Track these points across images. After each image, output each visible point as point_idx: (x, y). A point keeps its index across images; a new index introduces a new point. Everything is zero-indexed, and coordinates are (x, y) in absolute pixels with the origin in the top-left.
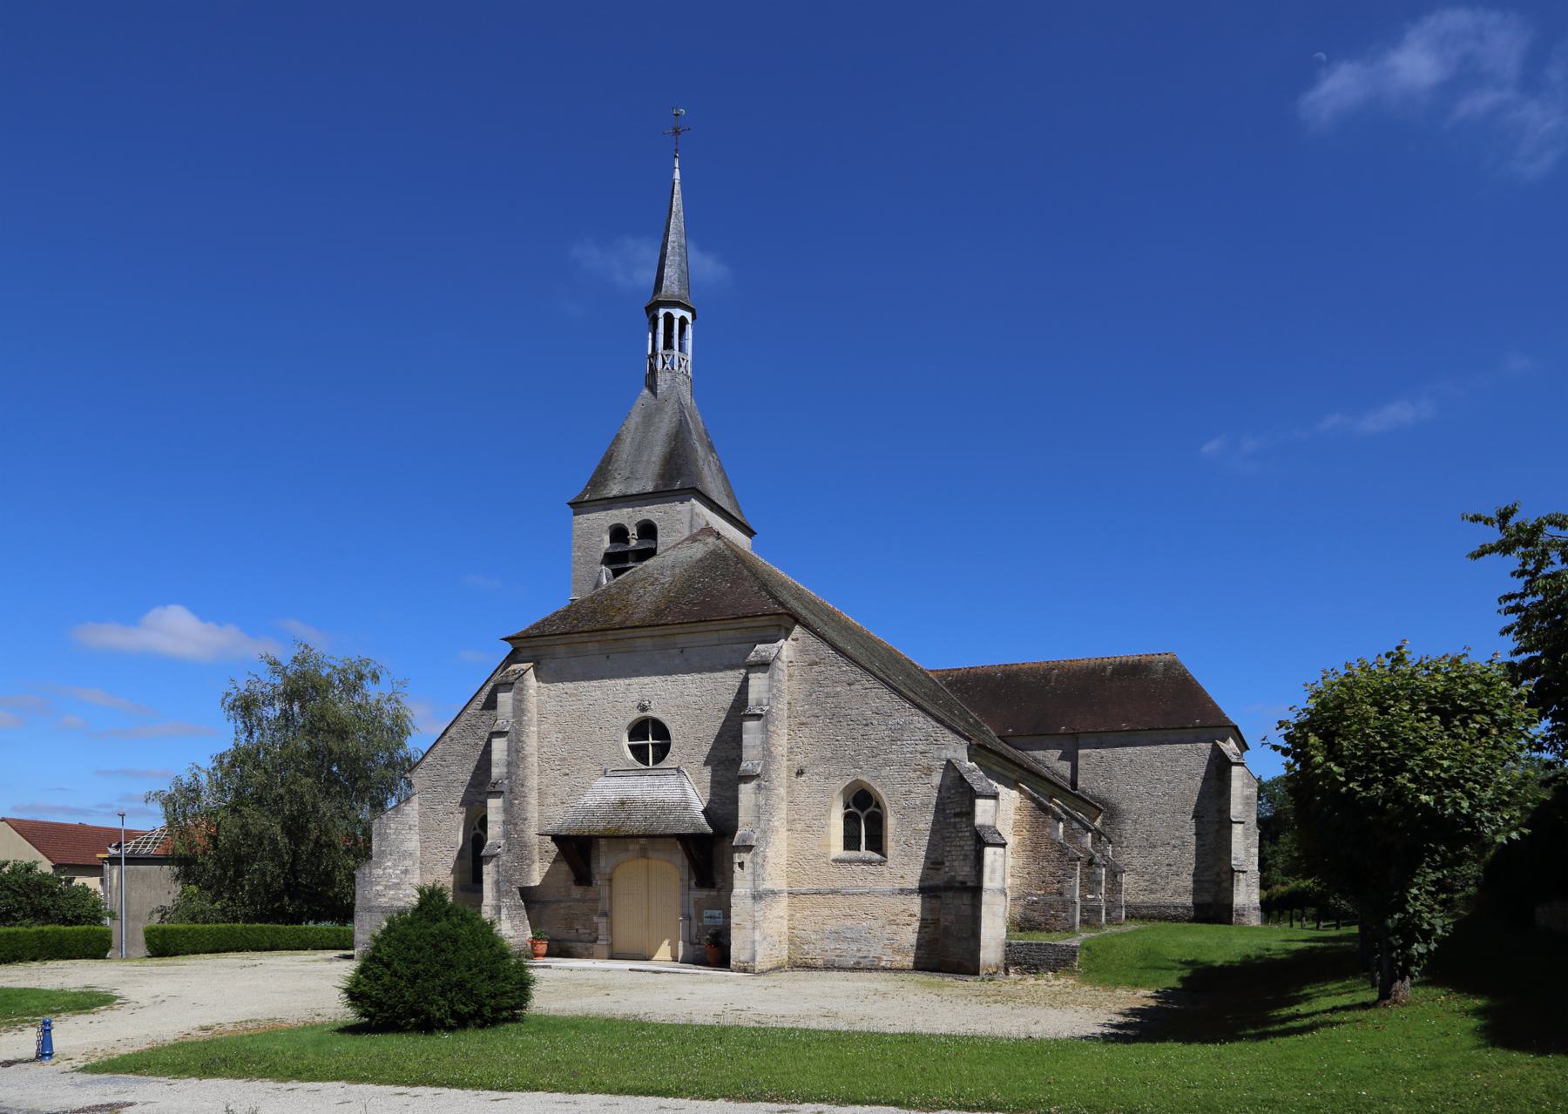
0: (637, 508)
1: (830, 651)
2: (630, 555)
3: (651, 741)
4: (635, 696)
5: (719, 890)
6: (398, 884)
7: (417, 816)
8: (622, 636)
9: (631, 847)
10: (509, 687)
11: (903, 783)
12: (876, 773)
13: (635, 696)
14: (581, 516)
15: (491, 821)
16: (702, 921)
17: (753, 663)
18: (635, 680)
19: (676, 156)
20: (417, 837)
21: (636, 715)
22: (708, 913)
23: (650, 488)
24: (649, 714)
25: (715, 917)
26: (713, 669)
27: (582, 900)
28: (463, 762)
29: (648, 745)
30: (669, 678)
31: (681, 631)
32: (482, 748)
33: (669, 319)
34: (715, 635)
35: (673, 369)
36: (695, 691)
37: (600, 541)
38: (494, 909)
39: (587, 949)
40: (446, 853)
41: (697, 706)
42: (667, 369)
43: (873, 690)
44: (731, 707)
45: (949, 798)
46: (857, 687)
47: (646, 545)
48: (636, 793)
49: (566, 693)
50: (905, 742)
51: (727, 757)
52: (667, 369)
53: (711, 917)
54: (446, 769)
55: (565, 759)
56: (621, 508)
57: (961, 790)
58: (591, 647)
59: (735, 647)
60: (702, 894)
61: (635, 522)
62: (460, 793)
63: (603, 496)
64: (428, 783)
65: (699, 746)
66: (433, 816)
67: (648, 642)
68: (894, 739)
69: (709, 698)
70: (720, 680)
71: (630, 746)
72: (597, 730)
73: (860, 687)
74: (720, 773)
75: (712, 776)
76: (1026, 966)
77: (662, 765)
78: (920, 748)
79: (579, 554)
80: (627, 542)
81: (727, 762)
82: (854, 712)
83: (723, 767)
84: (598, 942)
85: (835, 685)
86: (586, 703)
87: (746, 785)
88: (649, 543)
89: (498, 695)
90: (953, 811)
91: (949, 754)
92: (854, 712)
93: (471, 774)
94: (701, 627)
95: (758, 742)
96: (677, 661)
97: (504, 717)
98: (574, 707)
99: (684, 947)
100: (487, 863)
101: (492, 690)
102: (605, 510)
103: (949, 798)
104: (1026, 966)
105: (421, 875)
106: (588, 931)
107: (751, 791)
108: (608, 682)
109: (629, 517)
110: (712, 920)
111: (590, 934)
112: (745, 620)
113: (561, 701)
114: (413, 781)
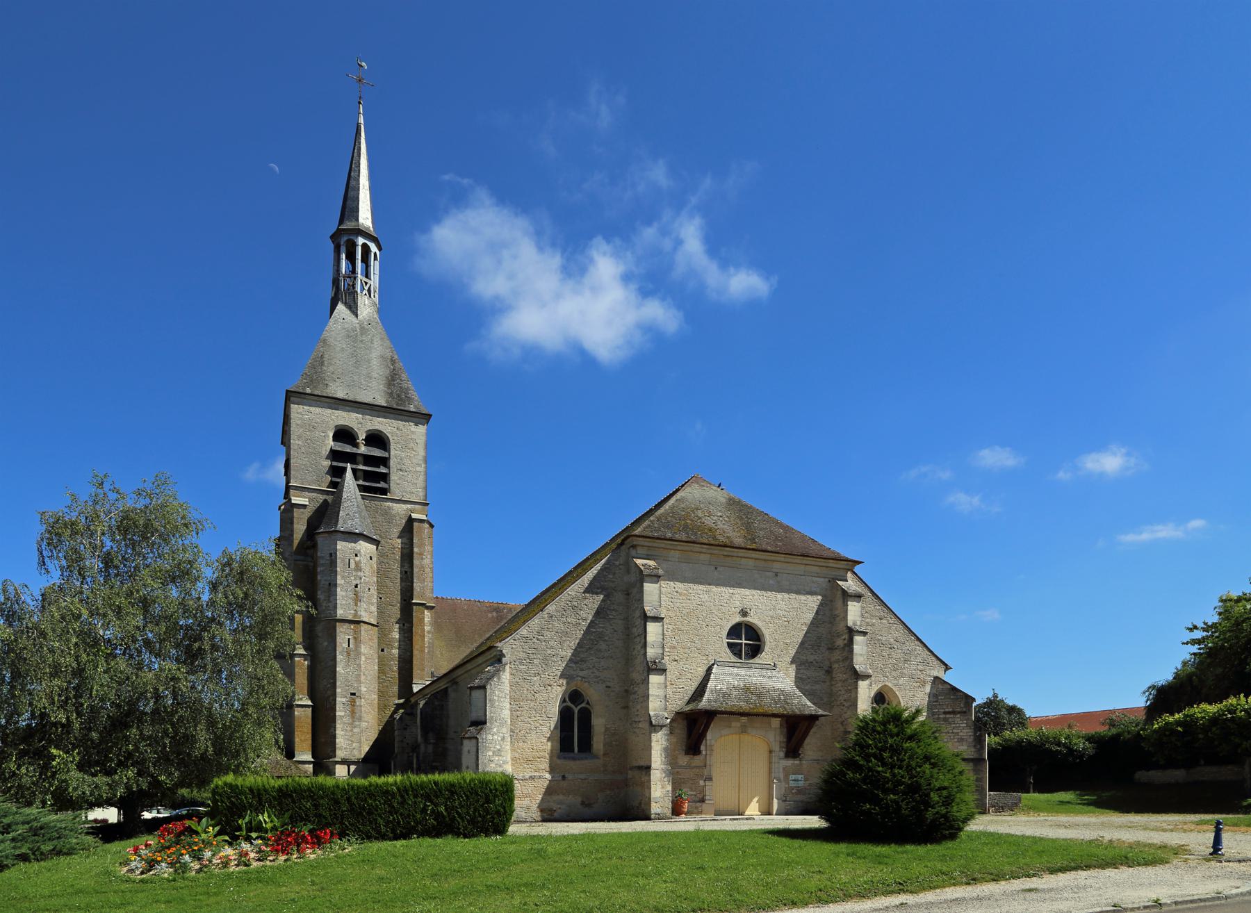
2: (360, 459)
4: (737, 605)
6: (499, 750)
8: (735, 554)
9: (733, 724)
10: (655, 579)
11: (910, 690)
13: (738, 604)
15: (653, 695)
16: (788, 783)
18: (737, 590)
19: (360, 103)
20: (508, 706)
21: (738, 619)
22: (793, 777)
23: (382, 402)
24: (747, 619)
25: (798, 780)
26: (798, 592)
27: (689, 767)
28: (564, 638)
29: (741, 644)
30: (764, 593)
32: (585, 628)
33: (366, 249)
34: (802, 567)
35: (370, 296)
38: (665, 772)
39: (696, 808)
42: (366, 294)
45: (935, 702)
47: (377, 452)
48: (754, 681)
49: (677, 592)
52: (366, 294)
53: (795, 780)
54: (544, 643)
55: (675, 648)
56: (349, 411)
58: (704, 557)
60: (790, 762)
61: (366, 430)
63: (330, 395)
64: (522, 655)
67: (751, 562)
69: (795, 614)
71: (728, 643)
72: (704, 626)
74: (802, 671)
77: (756, 660)
78: (920, 667)
79: (300, 443)
80: (356, 445)
82: (884, 638)
83: (803, 667)
84: (707, 802)
86: (694, 602)
89: (645, 584)
90: (943, 711)
91: (935, 673)
92: (884, 638)
93: (572, 651)
94: (798, 560)
95: (864, 652)
96: (771, 582)
97: (650, 605)
98: (685, 605)
100: (656, 731)
103: (936, 701)
106: (695, 793)
108: (714, 589)
109: (361, 424)
110: (796, 782)
113: (672, 598)
114: (504, 651)
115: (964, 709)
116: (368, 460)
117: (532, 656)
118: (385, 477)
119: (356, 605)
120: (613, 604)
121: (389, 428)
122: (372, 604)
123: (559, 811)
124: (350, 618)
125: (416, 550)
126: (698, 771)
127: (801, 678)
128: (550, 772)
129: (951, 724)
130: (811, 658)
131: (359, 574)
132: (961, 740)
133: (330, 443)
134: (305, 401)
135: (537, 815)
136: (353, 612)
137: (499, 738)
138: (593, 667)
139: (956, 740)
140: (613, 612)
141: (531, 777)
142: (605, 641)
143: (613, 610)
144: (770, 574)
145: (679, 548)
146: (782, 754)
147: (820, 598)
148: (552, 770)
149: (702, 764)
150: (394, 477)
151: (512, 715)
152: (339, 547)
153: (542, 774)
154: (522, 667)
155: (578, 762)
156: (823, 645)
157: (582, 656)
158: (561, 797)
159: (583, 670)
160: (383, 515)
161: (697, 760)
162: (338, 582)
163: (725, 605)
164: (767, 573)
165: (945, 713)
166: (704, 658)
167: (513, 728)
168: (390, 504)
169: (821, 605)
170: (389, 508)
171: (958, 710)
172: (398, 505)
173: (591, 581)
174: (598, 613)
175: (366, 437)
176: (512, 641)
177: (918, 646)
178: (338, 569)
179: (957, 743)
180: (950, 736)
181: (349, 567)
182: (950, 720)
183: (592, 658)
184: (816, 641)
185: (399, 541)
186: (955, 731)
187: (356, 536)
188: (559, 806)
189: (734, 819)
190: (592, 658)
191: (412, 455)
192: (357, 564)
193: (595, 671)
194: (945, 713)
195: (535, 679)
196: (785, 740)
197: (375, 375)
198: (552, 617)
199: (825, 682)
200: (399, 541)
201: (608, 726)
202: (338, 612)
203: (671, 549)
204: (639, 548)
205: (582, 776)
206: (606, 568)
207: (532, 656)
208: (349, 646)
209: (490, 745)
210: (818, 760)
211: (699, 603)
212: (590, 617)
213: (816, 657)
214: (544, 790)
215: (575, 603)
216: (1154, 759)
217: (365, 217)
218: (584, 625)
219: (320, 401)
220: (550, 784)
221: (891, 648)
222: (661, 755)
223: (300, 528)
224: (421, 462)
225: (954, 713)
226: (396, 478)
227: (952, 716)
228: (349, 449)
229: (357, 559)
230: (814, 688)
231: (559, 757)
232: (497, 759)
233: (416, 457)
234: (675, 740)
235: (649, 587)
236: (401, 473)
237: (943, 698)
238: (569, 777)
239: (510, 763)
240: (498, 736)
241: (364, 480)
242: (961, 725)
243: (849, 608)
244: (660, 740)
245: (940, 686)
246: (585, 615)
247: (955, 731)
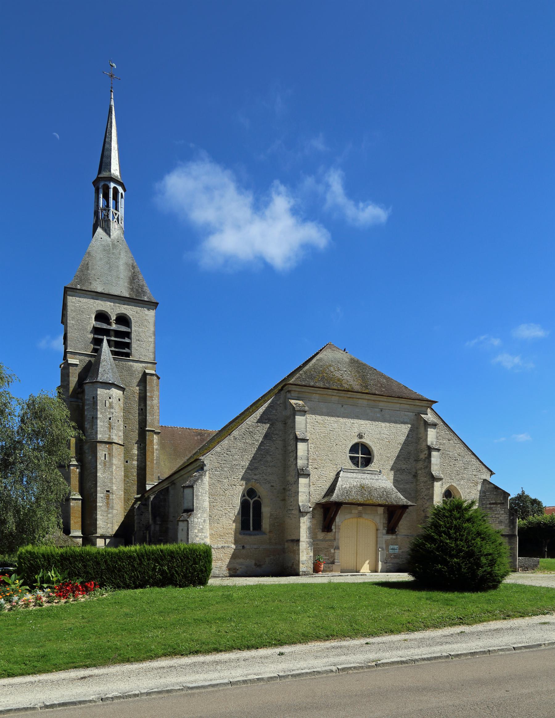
0: (117, 305)
1: (442, 423)
3: (360, 455)
4: (356, 431)
5: (396, 535)
6: (202, 529)
7: (208, 485)
8: (354, 397)
9: (353, 511)
10: (303, 413)
12: (458, 483)
14: (74, 298)
17: (431, 424)
18: (356, 421)
19: (111, 91)
20: (208, 499)
21: (356, 440)
22: (391, 547)
26: (396, 422)
27: (324, 540)
28: (244, 453)
29: (358, 457)
30: (374, 423)
31: (386, 400)
32: (257, 447)
34: (398, 405)
35: (118, 223)
36: (387, 432)
37: (89, 318)
40: (229, 510)
41: (387, 440)
42: (116, 222)
43: (458, 444)
44: (404, 443)
45: (485, 496)
46: (451, 442)
47: (123, 329)
49: (317, 422)
50: (469, 470)
51: (401, 468)
52: (116, 222)
54: (231, 457)
55: (315, 460)
56: (105, 301)
57: (495, 493)
59: (406, 413)
60: (389, 537)
61: (116, 313)
62: (242, 472)
63: (93, 290)
64: (217, 465)
65: (388, 460)
66: (220, 486)
67: (365, 402)
68: (465, 468)
70: (399, 429)
71: (350, 457)
72: (334, 445)
73: (452, 442)
75: (394, 477)
76: (523, 568)
77: (368, 468)
78: (474, 473)
80: (109, 324)
81: (401, 471)
82: (451, 453)
83: (399, 473)
84: (336, 564)
85: (443, 439)
87: (437, 483)
88: (126, 329)
91: (485, 477)
95: (438, 463)
96: (378, 415)
97: (300, 431)
99: (382, 564)
100: (303, 516)
101: (264, 412)
102: (93, 299)
103: (485, 496)
104: (523, 568)
105: (210, 524)
106: (328, 558)
107: (439, 486)
108: (341, 420)
111: (328, 559)
112: (417, 401)
114: (205, 462)
115: (503, 501)
116: (118, 334)
117: (223, 465)
118: (128, 345)
119: (110, 431)
120: (275, 430)
121: (131, 312)
122: (120, 431)
123: (240, 569)
124: (106, 440)
125: (148, 394)
126: (330, 542)
127: (397, 480)
128: (235, 544)
129: (494, 511)
130: (404, 467)
131: (112, 410)
132: (501, 522)
133: (93, 322)
134: (77, 294)
135: (226, 573)
137: (202, 521)
138: (263, 473)
139: (497, 522)
140: (276, 435)
141: (223, 546)
142: (270, 455)
143: (275, 434)
144: (377, 410)
145: (318, 392)
146: (385, 532)
147: (409, 426)
148: (236, 542)
149: (332, 538)
150: (134, 345)
151: (210, 505)
152: (99, 392)
153: (229, 545)
154: (216, 473)
155: (252, 537)
156: (411, 458)
157: (256, 465)
158: (241, 560)
159: (256, 475)
160: (127, 371)
161: (330, 535)
162: (99, 416)
163: (348, 431)
164: (376, 409)
165: (490, 504)
166: (335, 467)
167: (211, 514)
168: (132, 363)
169: (410, 431)
170: (131, 366)
171: (499, 502)
172: (137, 364)
173: (262, 415)
174: (266, 436)
175: (116, 318)
176: (211, 455)
177: (473, 458)
178: (98, 407)
179: (498, 524)
180: (493, 520)
182: (494, 509)
183: (261, 466)
184: (407, 455)
185: (138, 388)
186: (496, 516)
187: (110, 385)
188: (240, 566)
189: (353, 575)
190: (261, 466)
191: (146, 330)
192: (111, 404)
193: (264, 475)
194: (490, 504)
195: (225, 481)
196: (386, 522)
197: (122, 276)
198: (236, 439)
199: (413, 483)
200: (138, 388)
201: (272, 513)
202: (98, 436)
203: (313, 393)
204: (292, 392)
205: (255, 547)
206: (271, 406)
207: (223, 465)
208: (105, 459)
210: (408, 535)
211: (332, 429)
212: (261, 439)
213: (407, 466)
214: (231, 556)
215: (251, 430)
217: (115, 169)
218: (257, 444)
219: (86, 294)
220: (234, 551)
221: (455, 460)
222: (306, 532)
223: (73, 380)
224: (152, 335)
225: (496, 504)
226: (135, 346)
227: (495, 506)
228: (105, 326)
229: (110, 400)
230: (405, 487)
231: (240, 534)
232: (200, 535)
233: (148, 331)
234: (316, 522)
235: (299, 418)
236: (139, 342)
237: (489, 493)
238: (247, 547)
239: (209, 538)
241: (115, 348)
242: (501, 512)
243: (429, 433)
244: (306, 522)
245: (487, 486)
246: (257, 438)
247: (496, 516)
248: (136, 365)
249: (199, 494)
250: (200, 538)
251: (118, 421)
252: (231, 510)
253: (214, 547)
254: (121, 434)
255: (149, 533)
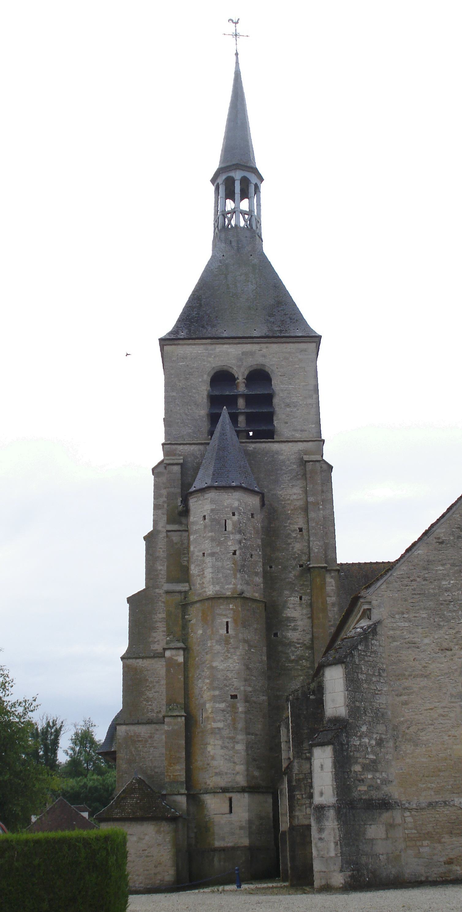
6: (374, 762)
122: (257, 574)
136: (231, 586)
137: (373, 742)
181: (226, 530)
208: (227, 632)
209: (357, 755)
216: (84, 803)
232: (370, 776)
240: (371, 738)
248: (283, 446)
249: (362, 677)
250: (370, 786)
251: (252, 555)
252: (446, 710)
253: (411, 807)
254: (259, 580)
255: (289, 782)
